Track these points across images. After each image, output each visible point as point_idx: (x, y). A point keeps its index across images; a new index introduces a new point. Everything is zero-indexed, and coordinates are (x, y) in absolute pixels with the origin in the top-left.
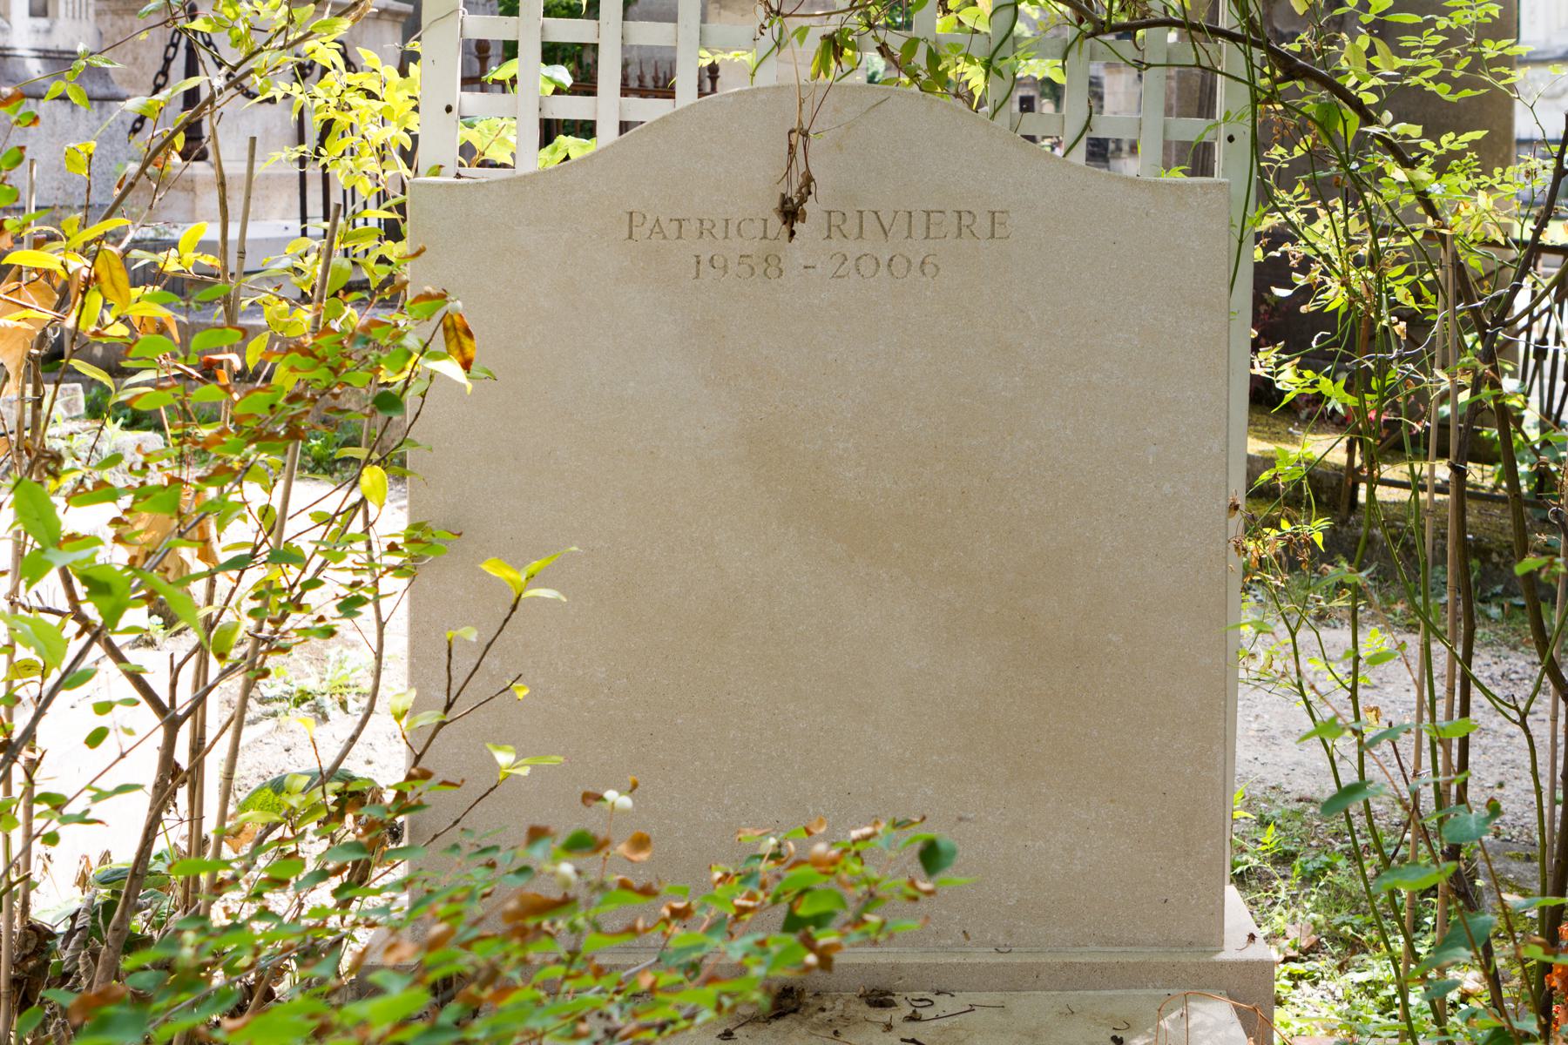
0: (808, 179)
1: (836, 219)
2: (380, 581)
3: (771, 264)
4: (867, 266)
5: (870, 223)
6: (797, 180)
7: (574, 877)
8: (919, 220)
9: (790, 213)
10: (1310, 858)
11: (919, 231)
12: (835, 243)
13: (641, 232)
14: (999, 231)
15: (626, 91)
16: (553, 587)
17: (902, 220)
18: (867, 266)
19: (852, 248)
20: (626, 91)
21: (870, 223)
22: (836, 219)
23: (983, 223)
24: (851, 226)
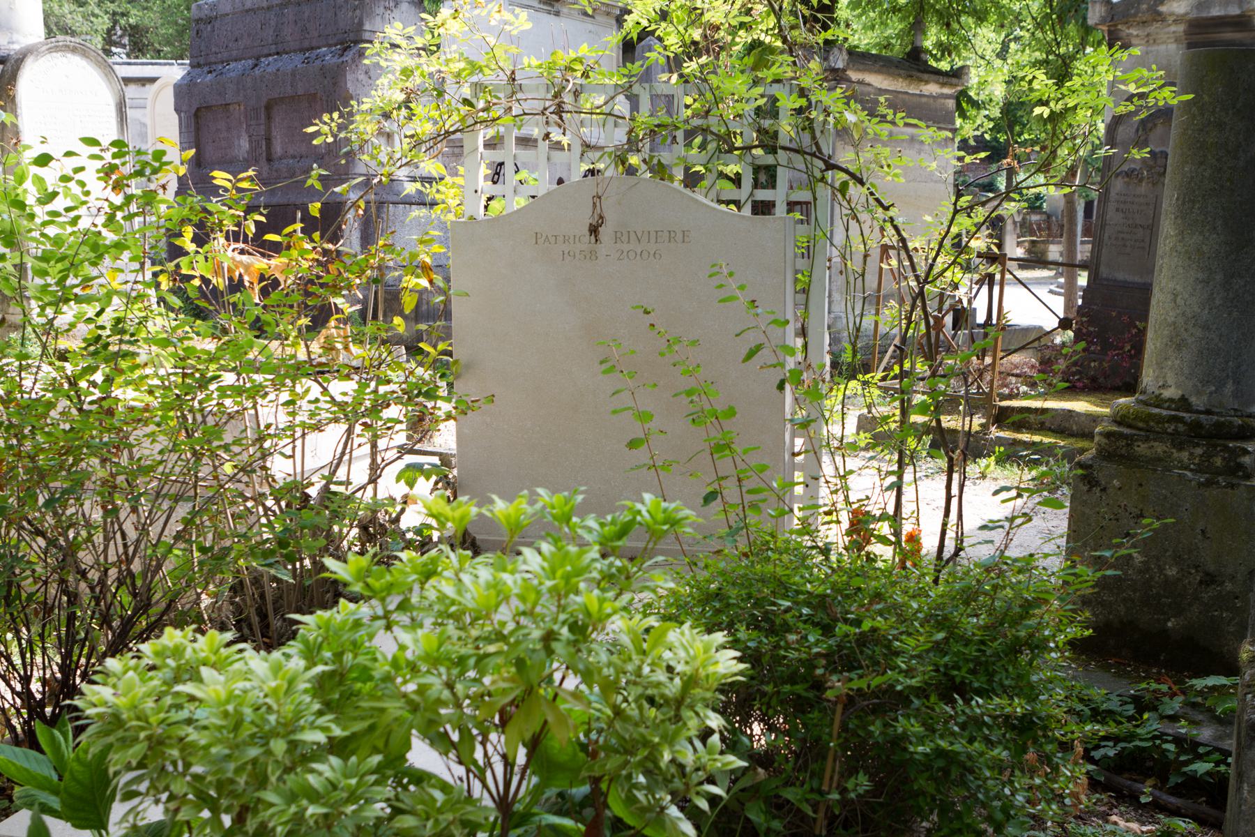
0: (601, 217)
1: (619, 235)
2: (365, 479)
3: (593, 255)
4: (632, 255)
5: (633, 236)
6: (596, 217)
7: (936, 811)
8: (653, 235)
9: (594, 230)
10: (130, 284)
11: (653, 240)
12: (618, 245)
13: (541, 241)
14: (686, 239)
15: (774, 187)
16: (1218, 674)
17: (646, 235)
18: (632, 255)
19: (626, 247)
20: (774, 187)
21: (633, 236)
22: (619, 235)
23: (680, 236)
24: (625, 238)
